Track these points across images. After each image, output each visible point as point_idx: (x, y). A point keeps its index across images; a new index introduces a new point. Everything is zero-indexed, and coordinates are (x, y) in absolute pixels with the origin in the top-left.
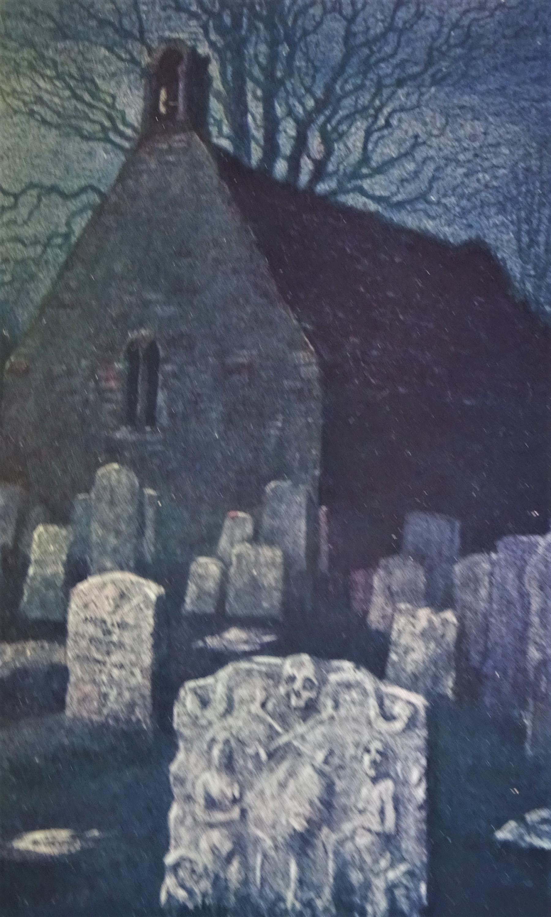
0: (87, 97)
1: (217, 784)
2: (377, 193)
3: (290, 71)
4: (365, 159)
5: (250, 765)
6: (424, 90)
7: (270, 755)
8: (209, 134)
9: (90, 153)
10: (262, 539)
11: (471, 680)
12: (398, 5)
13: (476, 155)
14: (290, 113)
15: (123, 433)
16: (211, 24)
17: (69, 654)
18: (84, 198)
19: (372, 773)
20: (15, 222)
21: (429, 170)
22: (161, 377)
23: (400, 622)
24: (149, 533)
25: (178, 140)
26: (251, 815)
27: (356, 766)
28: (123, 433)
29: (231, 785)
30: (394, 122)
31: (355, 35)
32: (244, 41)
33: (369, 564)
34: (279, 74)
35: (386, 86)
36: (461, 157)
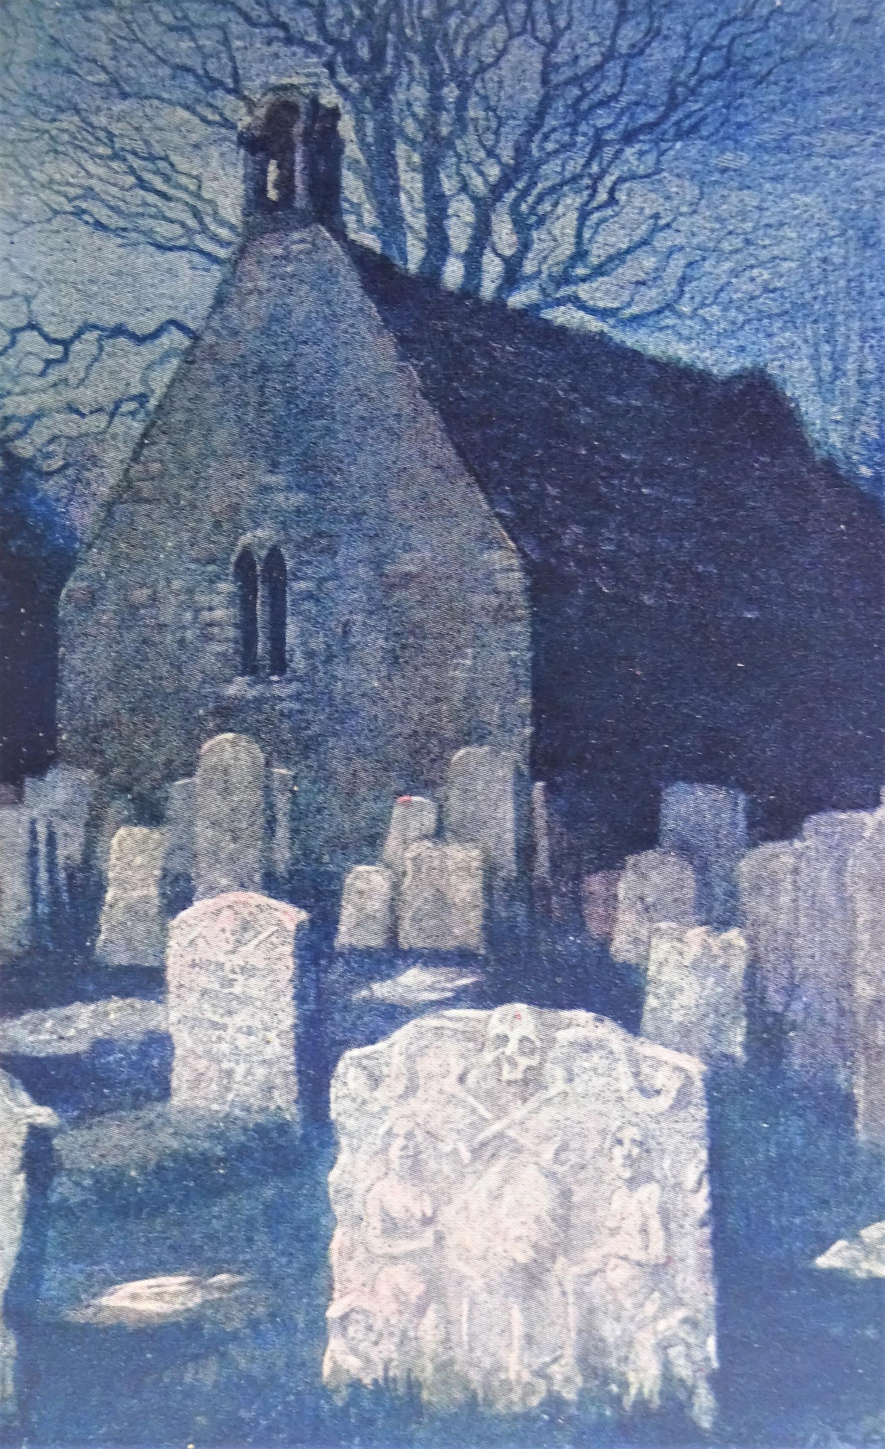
0: (158, 183)
1: (401, 1199)
2: (601, 304)
3: (461, 122)
4: (580, 255)
5: (447, 1169)
6: (664, 145)
7: (476, 1152)
8: (344, 225)
9: (169, 271)
10: (449, 835)
11: (769, 1034)
12: (622, 16)
13: (748, 242)
14: (464, 187)
15: (237, 688)
16: (339, 59)
17: (171, 1015)
18: (165, 340)
19: (627, 1174)
20: (65, 381)
21: (676, 267)
22: (289, 599)
23: (661, 949)
24: (282, 833)
25: (298, 240)
26: (450, 1241)
27: (602, 1162)
28: (237, 688)
29: (418, 1198)
30: (621, 196)
31: (557, 67)
32: (389, 84)
33: (611, 862)
34: (445, 131)
35: (608, 143)
36: (726, 246)
